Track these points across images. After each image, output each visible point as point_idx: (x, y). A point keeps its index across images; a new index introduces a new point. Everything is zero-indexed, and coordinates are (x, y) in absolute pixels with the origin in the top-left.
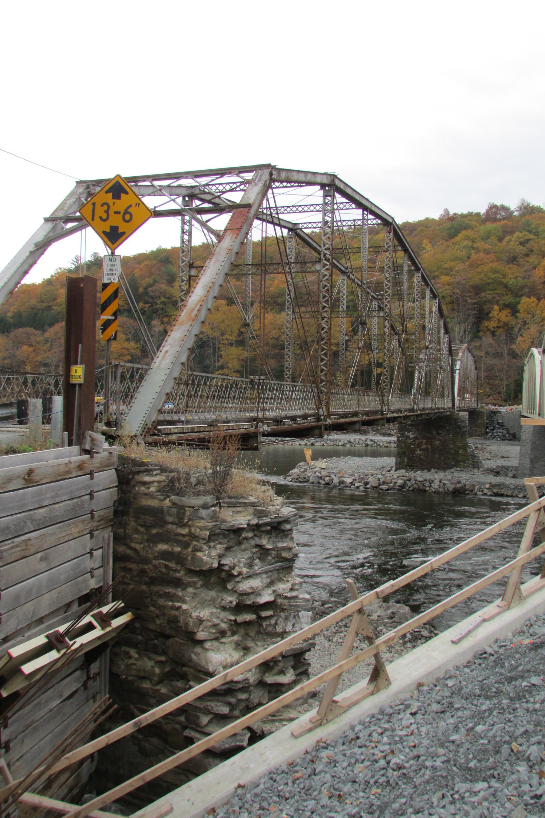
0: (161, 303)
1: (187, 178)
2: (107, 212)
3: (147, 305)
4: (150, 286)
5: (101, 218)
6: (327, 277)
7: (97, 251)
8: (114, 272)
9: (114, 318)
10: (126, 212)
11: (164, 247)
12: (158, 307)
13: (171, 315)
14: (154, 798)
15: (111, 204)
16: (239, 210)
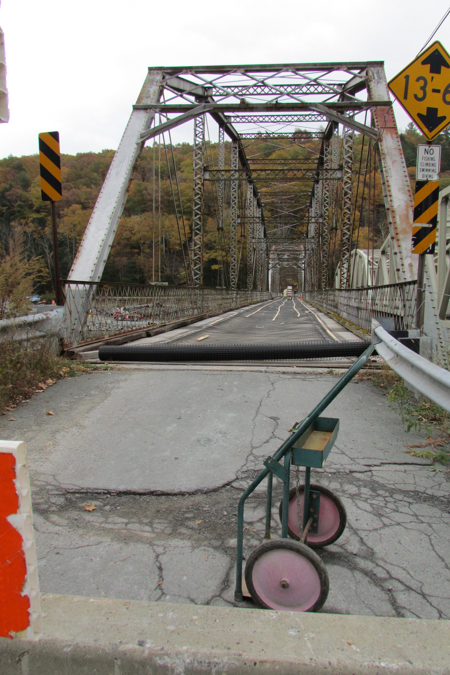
0: (18, 206)
1: (287, 71)
2: (423, 88)
3: (5, 208)
4: (6, 190)
5: (416, 96)
6: (199, 186)
8: (431, 168)
11: (14, 156)
12: (15, 209)
13: (28, 218)
15: (429, 80)
16: (379, 107)
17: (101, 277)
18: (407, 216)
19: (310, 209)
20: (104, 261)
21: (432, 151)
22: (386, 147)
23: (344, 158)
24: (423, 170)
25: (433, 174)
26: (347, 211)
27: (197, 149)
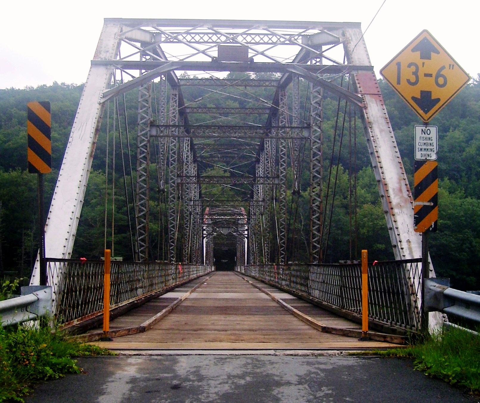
7: (412, 96)
8: (429, 147)
9: (432, 204)
10: (438, 75)
14: (467, 326)
15: (420, 66)
17: (71, 254)
18: (400, 190)
19: (257, 165)
20: (73, 235)
21: (428, 131)
22: (372, 115)
23: (311, 115)
24: (421, 150)
25: (432, 153)
26: (316, 174)
27: (143, 101)
